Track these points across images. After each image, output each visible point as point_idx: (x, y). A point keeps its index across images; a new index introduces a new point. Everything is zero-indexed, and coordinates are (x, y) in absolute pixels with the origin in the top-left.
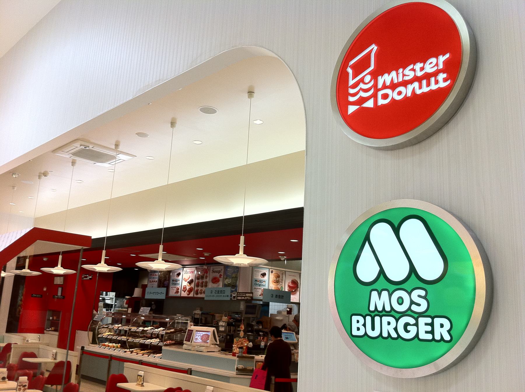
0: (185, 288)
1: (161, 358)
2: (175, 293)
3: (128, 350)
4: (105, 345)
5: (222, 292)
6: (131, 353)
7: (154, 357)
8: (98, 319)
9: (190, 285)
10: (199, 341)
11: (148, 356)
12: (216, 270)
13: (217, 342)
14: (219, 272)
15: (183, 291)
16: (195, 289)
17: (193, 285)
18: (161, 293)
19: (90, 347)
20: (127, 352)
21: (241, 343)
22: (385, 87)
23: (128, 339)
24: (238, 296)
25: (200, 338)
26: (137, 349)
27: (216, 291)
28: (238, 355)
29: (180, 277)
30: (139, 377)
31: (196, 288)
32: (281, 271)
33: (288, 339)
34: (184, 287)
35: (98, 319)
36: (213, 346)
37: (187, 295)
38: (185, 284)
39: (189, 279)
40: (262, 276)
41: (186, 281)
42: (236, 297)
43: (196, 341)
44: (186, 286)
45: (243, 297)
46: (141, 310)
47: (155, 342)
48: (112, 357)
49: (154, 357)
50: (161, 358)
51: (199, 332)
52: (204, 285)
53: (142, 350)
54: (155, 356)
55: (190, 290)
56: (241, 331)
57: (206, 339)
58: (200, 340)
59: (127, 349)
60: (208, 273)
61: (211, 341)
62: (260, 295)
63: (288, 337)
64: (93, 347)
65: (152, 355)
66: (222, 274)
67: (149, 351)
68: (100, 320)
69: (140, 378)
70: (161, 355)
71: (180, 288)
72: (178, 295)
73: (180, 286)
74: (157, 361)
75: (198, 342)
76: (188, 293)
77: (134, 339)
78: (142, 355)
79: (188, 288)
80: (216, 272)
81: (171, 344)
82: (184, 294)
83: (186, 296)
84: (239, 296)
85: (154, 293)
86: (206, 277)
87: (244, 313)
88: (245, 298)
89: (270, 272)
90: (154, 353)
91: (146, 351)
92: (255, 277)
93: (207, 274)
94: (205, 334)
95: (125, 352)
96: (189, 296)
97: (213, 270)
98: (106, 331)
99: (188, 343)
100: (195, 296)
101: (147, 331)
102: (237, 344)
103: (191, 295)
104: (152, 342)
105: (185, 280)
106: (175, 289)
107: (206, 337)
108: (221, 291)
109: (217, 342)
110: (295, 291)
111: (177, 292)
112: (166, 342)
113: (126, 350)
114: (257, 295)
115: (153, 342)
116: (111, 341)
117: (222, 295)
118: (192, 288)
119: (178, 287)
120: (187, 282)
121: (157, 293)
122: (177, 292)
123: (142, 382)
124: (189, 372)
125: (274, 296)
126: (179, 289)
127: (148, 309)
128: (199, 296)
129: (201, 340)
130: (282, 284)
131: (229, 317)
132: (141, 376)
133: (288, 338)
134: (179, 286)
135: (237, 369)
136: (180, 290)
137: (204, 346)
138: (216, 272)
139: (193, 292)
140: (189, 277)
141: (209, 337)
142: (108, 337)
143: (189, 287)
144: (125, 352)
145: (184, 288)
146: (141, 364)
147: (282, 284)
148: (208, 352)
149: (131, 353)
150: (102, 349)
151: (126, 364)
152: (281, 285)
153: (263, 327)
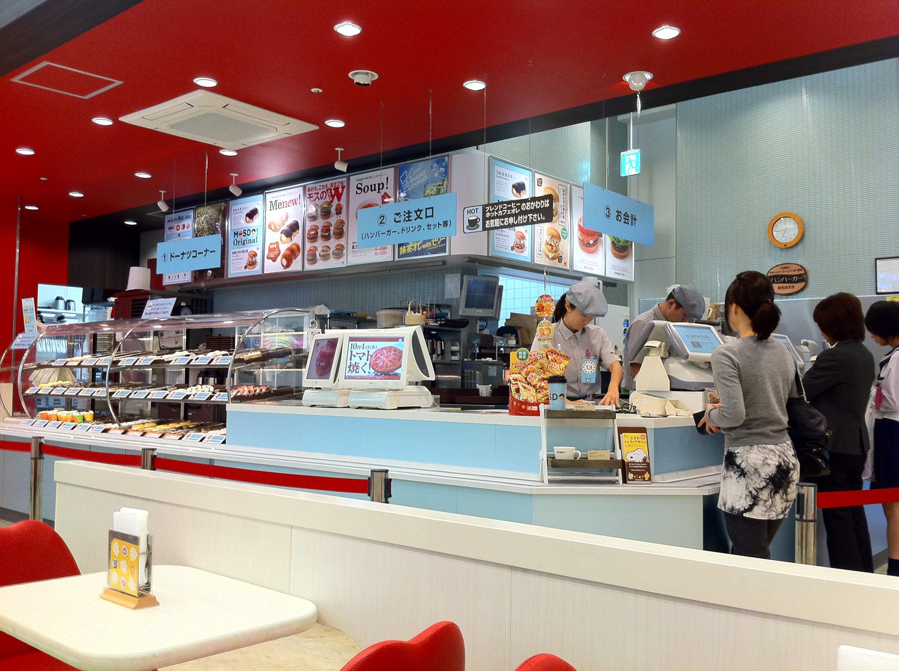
0: (274, 249)
1: (224, 442)
2: (246, 267)
3: (116, 425)
4: (48, 418)
5: (423, 213)
6: (123, 433)
7: (201, 441)
8: (24, 345)
9: (289, 239)
10: (367, 374)
11: (180, 439)
12: (365, 183)
13: (427, 375)
14: (381, 186)
15: (268, 259)
16: (307, 249)
17: (297, 238)
18: (206, 251)
19: (6, 425)
20: (110, 432)
21: (538, 365)
22: (412, 183)
23: (111, 394)
24: (490, 218)
25: (368, 363)
26: (145, 421)
27: (398, 214)
28: (547, 407)
29: (258, 221)
30: (116, 543)
31: (308, 245)
32: (560, 183)
33: (700, 346)
34: (272, 246)
35: (24, 345)
36: (413, 388)
37: (282, 268)
38: (274, 237)
39: (284, 222)
40: (515, 191)
41: (275, 230)
42: (480, 223)
43: (354, 374)
44: (277, 243)
45: (509, 216)
46: (147, 309)
47: (198, 393)
48: (41, 444)
49: (201, 441)
50: (224, 442)
51: (360, 343)
52: (332, 232)
53: (159, 424)
54: (204, 438)
55: (291, 255)
56: (542, 319)
57: (389, 364)
58: (367, 368)
59: (113, 423)
60: (344, 197)
61: (409, 372)
62: (513, 249)
63: (700, 340)
64: (15, 426)
65: (192, 433)
66: (390, 192)
67: (182, 424)
68: (28, 348)
69: (125, 552)
70: (223, 431)
71: (259, 253)
72: (256, 271)
73: (261, 248)
74: (213, 450)
75: (362, 378)
76: (285, 263)
77: (131, 391)
78: (161, 437)
79: (283, 248)
80: (372, 188)
81: (254, 395)
82: (274, 267)
83: (282, 270)
84: (494, 218)
85: (183, 254)
86: (339, 211)
87: (463, 303)
88: (517, 218)
89: (536, 183)
90: (198, 428)
91: (171, 425)
92: (497, 193)
93: (339, 200)
94: (383, 349)
95: (106, 431)
96: (288, 270)
97: (359, 186)
98: (50, 378)
99: (321, 383)
100: (309, 267)
101: (170, 362)
102: (525, 370)
103: (296, 266)
104: (188, 393)
105: (273, 228)
106: (245, 258)
107: (392, 356)
108: (416, 212)
109: (427, 375)
110: (595, 242)
111: (252, 264)
112: (239, 392)
113: (109, 426)
114: (506, 248)
115: (193, 393)
116: (69, 404)
117: (424, 222)
118: (298, 246)
119: (253, 248)
120: (280, 231)
121: (194, 254)
122: (252, 264)
123: (143, 580)
124: (378, 487)
125: (614, 214)
126: (255, 255)
127: (170, 304)
128: (320, 265)
129: (372, 371)
130: (564, 220)
131: (424, 312)
132: (135, 540)
133: (698, 343)
134: (256, 247)
135: (554, 464)
136: (259, 259)
137: (384, 390)
138: (372, 188)
139: (300, 257)
140: (284, 217)
141: (401, 357)
142: (53, 393)
143: (288, 245)
144: (106, 431)
145: (270, 250)
146: (730, 552)
147: (564, 220)
148: (399, 408)
149: (123, 433)
150: (37, 429)
151: (63, 468)
152: (562, 222)
153: (517, 342)
